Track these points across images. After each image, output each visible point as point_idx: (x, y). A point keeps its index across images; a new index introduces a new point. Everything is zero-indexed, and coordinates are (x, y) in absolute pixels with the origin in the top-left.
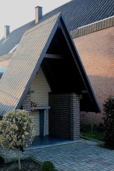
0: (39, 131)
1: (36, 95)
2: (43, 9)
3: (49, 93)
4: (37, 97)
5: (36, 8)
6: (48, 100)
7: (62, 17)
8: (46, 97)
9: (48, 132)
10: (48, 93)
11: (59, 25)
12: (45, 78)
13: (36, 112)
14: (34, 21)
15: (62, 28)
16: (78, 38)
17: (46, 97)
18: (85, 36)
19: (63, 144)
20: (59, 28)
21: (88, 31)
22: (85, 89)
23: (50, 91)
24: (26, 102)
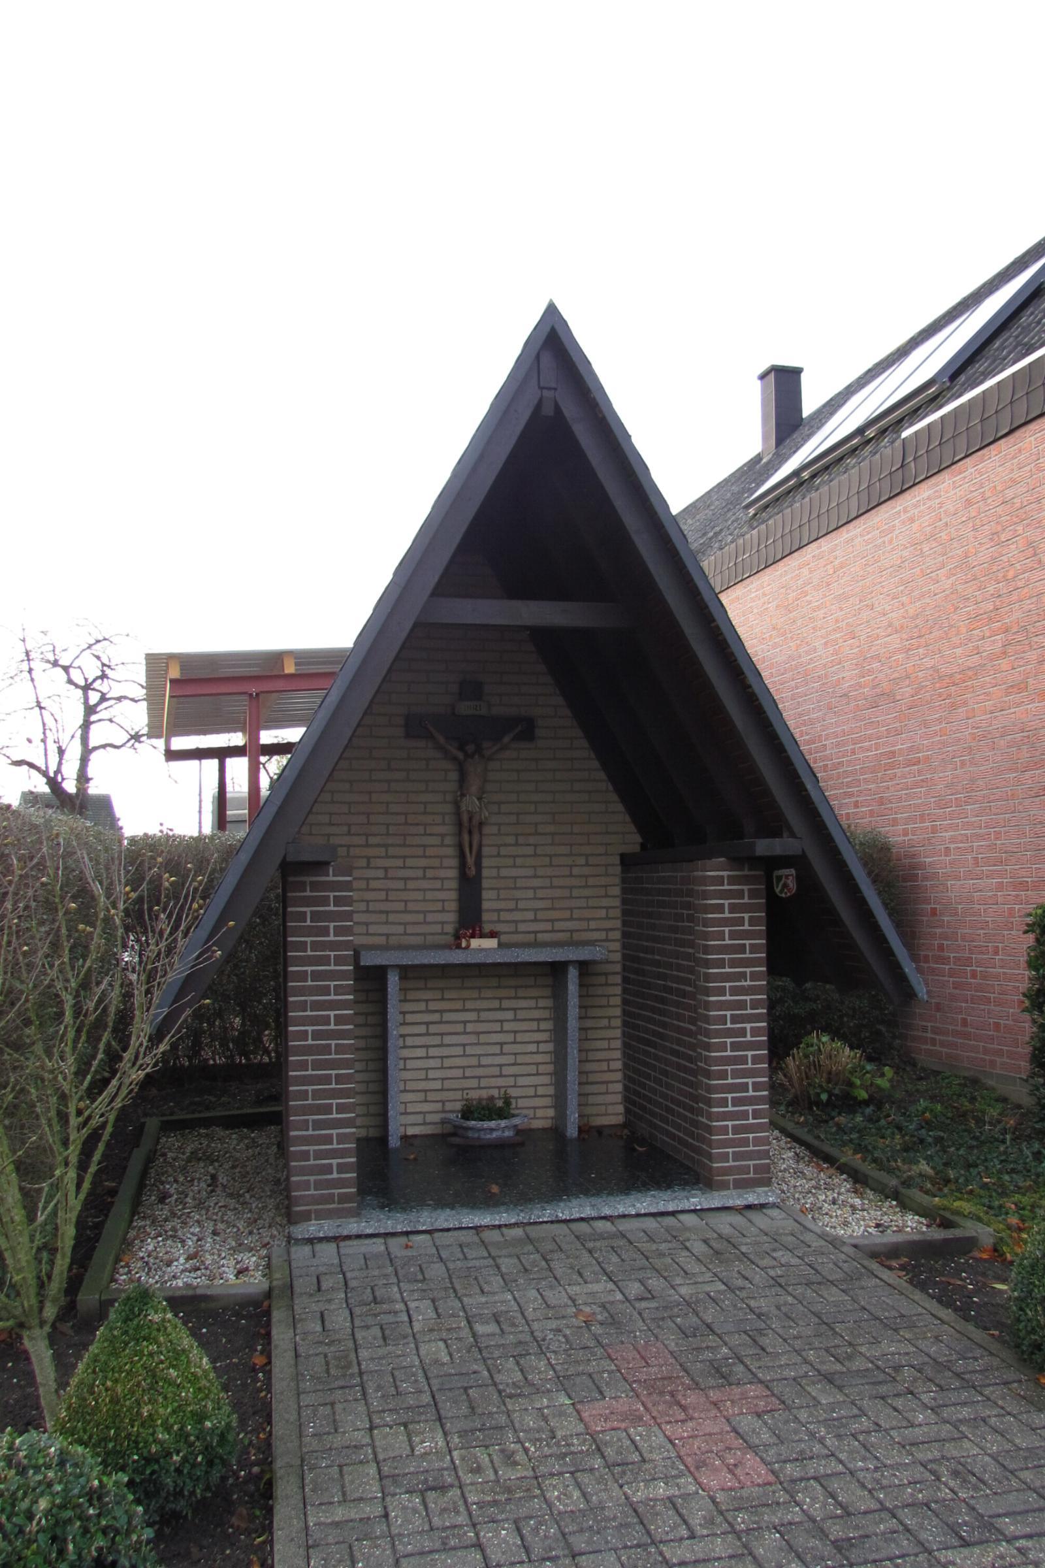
0: (548, 1101)
1: (530, 872)
2: (804, 377)
3: (626, 861)
4: (536, 882)
5: (762, 377)
6: (617, 902)
7: (557, 327)
8: (603, 881)
9: (620, 1109)
10: (617, 860)
11: (546, 393)
12: (596, 764)
13: (531, 981)
14: (758, 459)
15: (570, 410)
16: (907, 496)
17: (603, 881)
18: (945, 475)
19: (607, 1211)
20: (548, 410)
21: (962, 443)
22: (775, 827)
23: (632, 841)
24: (316, 916)
